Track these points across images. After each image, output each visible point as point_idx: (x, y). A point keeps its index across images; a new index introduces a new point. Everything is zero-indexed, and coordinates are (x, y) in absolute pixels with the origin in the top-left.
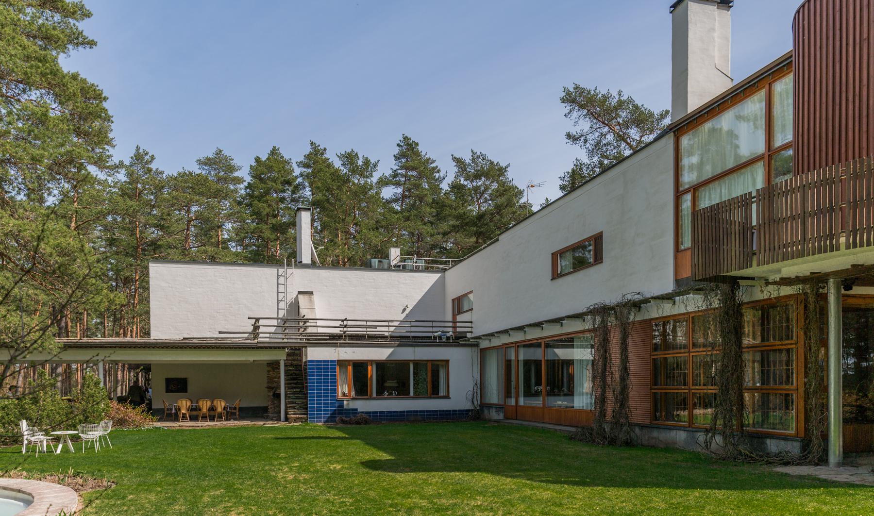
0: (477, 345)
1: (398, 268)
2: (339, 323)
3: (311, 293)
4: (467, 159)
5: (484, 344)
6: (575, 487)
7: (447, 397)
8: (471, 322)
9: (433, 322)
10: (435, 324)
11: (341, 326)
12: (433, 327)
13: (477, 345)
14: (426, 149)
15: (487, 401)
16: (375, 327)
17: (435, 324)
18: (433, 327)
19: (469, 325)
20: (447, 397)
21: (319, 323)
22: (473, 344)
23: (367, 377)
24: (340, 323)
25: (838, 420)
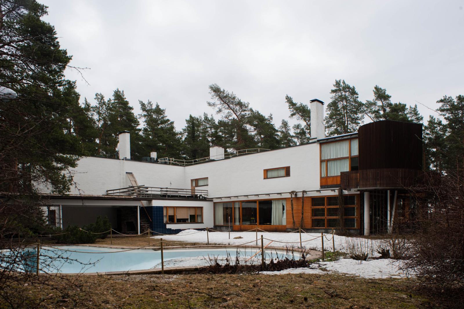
0: (212, 201)
1: (156, 162)
2: (160, 190)
3: (207, 178)
4: (146, 103)
5: (215, 201)
6: (376, 240)
7: (202, 223)
8: (207, 191)
9: (170, 189)
10: (202, 191)
11: (161, 191)
12: (152, 191)
13: (212, 201)
14: (128, 97)
15: (216, 225)
16: (177, 192)
17: (202, 191)
18: (152, 191)
19: (206, 192)
20: (202, 223)
21: (153, 189)
22: (211, 200)
23: (371, 207)
24: (160, 190)
25: (122, 273)
